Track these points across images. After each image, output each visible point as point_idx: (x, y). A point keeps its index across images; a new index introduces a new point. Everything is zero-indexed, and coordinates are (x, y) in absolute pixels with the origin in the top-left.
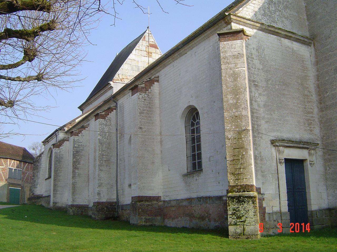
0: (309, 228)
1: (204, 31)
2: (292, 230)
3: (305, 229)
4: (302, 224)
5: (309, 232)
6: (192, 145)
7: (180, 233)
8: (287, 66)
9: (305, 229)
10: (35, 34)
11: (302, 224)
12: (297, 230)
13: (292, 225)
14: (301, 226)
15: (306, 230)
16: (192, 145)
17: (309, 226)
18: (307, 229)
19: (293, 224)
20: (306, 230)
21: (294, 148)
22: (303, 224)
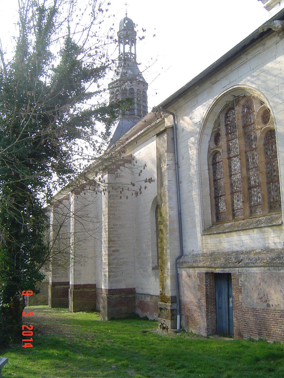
0: (27, 346)
1: (216, 189)
2: (25, 328)
3: (26, 342)
4: (31, 338)
5: (23, 346)
6: (71, 304)
7: (136, 35)
8: (144, 343)
9: (26, 342)
10: (182, 254)
11: (31, 338)
12: (25, 333)
13: (31, 327)
14: (29, 337)
15: (25, 344)
16: (71, 304)
17: (29, 346)
18: (26, 344)
19: (32, 328)
20: (25, 344)
21: (239, 62)
22: (31, 340)
